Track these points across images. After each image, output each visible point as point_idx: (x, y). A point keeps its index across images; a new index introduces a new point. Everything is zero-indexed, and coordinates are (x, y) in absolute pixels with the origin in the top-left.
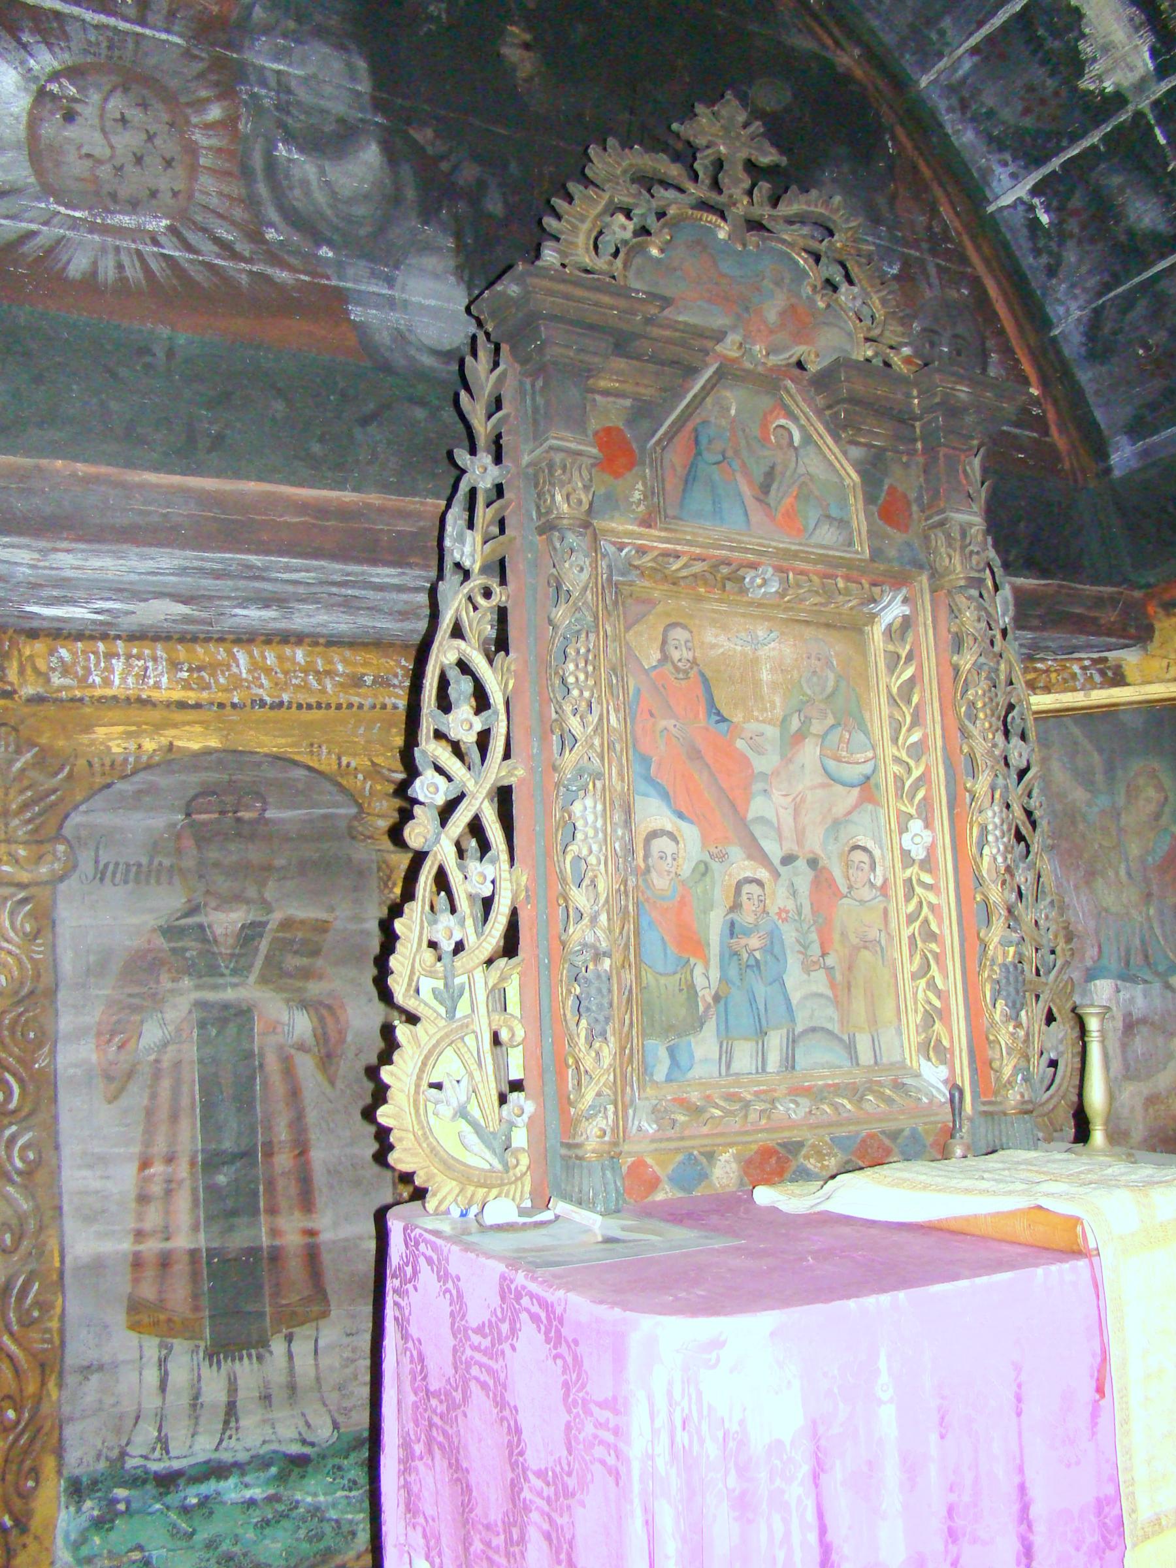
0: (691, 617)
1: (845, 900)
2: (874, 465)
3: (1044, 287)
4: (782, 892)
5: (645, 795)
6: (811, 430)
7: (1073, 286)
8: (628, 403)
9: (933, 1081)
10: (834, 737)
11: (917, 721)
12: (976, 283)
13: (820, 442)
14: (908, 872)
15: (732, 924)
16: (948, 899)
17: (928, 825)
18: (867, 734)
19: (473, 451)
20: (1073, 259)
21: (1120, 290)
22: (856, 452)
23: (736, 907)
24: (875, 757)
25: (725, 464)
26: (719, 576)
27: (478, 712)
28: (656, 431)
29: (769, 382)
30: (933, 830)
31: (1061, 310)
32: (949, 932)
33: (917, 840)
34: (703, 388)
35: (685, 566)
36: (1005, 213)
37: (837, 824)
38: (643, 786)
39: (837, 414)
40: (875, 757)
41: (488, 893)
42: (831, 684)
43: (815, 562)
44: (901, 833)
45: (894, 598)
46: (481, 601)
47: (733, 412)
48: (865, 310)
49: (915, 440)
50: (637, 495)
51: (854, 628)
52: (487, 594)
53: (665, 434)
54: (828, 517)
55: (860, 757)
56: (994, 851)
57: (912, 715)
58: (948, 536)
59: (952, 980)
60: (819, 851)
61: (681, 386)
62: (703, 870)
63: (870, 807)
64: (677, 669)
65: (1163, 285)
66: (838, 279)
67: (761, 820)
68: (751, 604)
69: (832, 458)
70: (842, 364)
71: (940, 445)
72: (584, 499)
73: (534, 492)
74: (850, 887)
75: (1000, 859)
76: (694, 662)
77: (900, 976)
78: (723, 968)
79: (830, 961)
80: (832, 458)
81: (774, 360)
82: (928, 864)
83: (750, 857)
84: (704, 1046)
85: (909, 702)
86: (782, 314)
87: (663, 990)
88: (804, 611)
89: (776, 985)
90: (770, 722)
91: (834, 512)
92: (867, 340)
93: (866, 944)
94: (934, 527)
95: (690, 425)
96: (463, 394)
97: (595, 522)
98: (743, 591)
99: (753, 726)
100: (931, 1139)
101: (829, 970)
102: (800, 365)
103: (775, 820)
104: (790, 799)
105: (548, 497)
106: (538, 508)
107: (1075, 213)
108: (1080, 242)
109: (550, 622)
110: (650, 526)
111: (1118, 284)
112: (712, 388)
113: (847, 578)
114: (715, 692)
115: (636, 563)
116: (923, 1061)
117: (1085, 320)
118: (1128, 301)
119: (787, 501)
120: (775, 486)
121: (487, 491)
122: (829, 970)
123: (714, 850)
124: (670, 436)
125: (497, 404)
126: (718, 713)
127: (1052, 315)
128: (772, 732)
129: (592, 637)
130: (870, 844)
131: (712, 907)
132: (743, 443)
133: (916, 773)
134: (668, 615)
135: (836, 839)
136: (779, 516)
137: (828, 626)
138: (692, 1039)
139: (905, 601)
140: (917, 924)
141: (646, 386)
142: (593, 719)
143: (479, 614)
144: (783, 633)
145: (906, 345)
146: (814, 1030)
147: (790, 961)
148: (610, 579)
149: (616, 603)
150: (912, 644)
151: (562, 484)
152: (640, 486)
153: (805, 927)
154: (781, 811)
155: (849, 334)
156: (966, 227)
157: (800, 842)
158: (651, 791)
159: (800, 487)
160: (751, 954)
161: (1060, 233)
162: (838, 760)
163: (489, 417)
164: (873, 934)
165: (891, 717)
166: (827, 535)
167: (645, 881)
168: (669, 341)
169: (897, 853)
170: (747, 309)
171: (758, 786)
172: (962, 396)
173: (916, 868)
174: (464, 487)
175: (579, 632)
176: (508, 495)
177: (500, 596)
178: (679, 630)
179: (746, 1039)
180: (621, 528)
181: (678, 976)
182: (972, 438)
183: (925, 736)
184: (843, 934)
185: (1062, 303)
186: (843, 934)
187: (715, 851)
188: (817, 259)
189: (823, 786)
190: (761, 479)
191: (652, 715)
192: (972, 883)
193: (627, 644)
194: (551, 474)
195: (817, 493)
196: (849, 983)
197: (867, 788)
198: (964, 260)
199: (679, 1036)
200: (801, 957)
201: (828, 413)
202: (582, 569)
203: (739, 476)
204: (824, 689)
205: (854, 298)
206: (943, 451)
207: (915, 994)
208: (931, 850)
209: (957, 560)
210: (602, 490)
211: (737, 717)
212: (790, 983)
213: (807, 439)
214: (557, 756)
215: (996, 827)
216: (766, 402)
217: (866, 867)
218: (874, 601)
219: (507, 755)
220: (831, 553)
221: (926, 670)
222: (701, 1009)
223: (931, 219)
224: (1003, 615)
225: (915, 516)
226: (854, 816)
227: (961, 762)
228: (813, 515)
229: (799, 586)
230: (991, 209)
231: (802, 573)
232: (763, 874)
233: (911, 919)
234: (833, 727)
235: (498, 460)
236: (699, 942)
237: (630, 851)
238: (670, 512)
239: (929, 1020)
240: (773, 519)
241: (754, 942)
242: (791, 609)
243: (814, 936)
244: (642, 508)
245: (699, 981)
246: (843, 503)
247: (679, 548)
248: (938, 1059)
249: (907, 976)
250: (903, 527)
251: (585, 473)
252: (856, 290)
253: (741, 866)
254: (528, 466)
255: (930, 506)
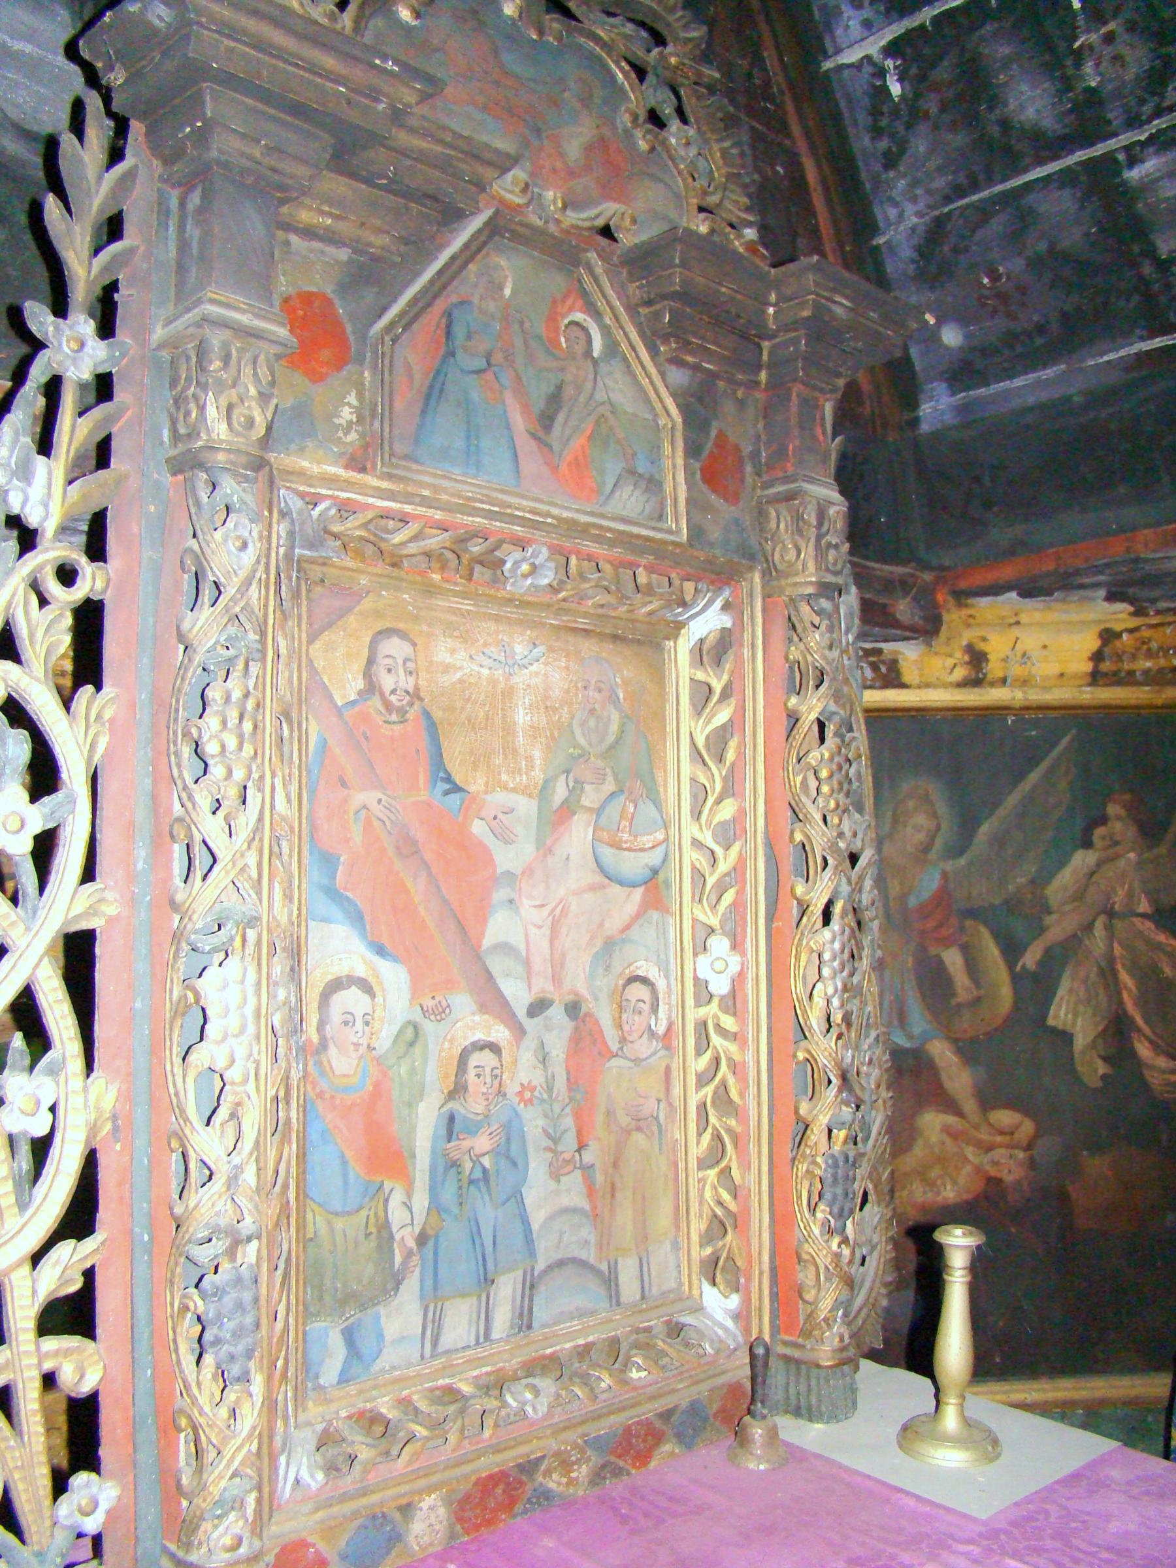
0: (416, 618)
1: (614, 1062)
2: (700, 400)
3: (877, 182)
4: (527, 1056)
5: (326, 920)
6: (620, 336)
7: (916, 182)
8: (343, 254)
9: (719, 1316)
10: (613, 810)
11: (731, 788)
12: (794, 163)
13: (630, 355)
14: (702, 1011)
15: (452, 1119)
16: (756, 1057)
17: (737, 946)
18: (658, 804)
19: (60, 309)
20: (922, 149)
21: (975, 197)
22: (678, 376)
23: (458, 1090)
24: (666, 840)
25: (489, 376)
26: (465, 558)
27: (35, 797)
28: (384, 309)
29: (562, 252)
30: (743, 954)
31: (892, 213)
32: (756, 1104)
33: (719, 965)
34: (466, 246)
35: (414, 538)
36: (846, 74)
37: (609, 946)
38: (323, 905)
39: (657, 315)
40: (666, 840)
41: (42, 1131)
42: (614, 728)
43: (612, 544)
44: (695, 954)
45: (711, 602)
46: (53, 587)
47: (507, 292)
48: (701, 163)
49: (759, 368)
50: (347, 414)
51: (648, 640)
52: (67, 575)
53: (402, 314)
54: (632, 472)
55: (646, 840)
56: (830, 991)
57: (725, 779)
58: (798, 518)
59: (756, 1179)
60: (584, 992)
61: (432, 238)
62: (411, 1036)
63: (655, 915)
64: (388, 706)
65: (1030, 199)
66: (668, 111)
67: (505, 948)
68: (509, 601)
69: (645, 382)
70: (674, 237)
71: (795, 380)
72: (259, 419)
73: (168, 397)
74: (623, 1040)
75: (836, 1002)
76: (415, 695)
77: (681, 1165)
78: (433, 1189)
79: (588, 1157)
80: (645, 382)
81: (573, 218)
82: (733, 1002)
83: (483, 1008)
84: (400, 1318)
85: (721, 759)
86: (588, 149)
87: (339, 1239)
88: (585, 615)
89: (511, 1206)
90: (525, 791)
91: (642, 467)
92: (701, 209)
93: (639, 1123)
94: (777, 500)
95: (440, 305)
96: (51, 202)
97: (272, 457)
98: (498, 580)
99: (499, 798)
100: (715, 1407)
101: (587, 1169)
102: (606, 232)
103: (522, 947)
104: (546, 911)
105: (192, 406)
106: (174, 423)
107: (936, 88)
108: (936, 128)
109: (181, 637)
110: (363, 470)
111: (975, 187)
112: (479, 250)
113: (650, 569)
114: (445, 745)
115: (336, 528)
116: (706, 1287)
117: (921, 230)
118: (984, 213)
119: (578, 442)
120: (561, 418)
121: (83, 386)
122: (587, 1169)
123: (429, 1003)
124: (409, 319)
125: (113, 228)
126: (448, 779)
127: (880, 218)
128: (526, 806)
129: (254, 669)
130: (653, 973)
131: (422, 1096)
132: (519, 342)
133: (723, 867)
134: (378, 614)
135: (608, 968)
136: (563, 467)
137: (615, 638)
138: (382, 1310)
139: (726, 607)
140: (709, 1090)
141: (379, 231)
142: (246, 821)
143: (50, 612)
144: (551, 649)
145: (750, 224)
146: (561, 1263)
147: (532, 1165)
148: (289, 556)
149: (296, 595)
150: (732, 673)
151: (221, 387)
152: (352, 399)
153: (557, 1108)
154: (533, 931)
155: (677, 196)
156: (792, 86)
157: (556, 979)
158: (339, 915)
159: (597, 423)
160: (476, 1161)
161: (911, 111)
162: (617, 845)
163: (97, 251)
164: (649, 1107)
165: (693, 780)
166: (629, 502)
167: (319, 1063)
168: (422, 157)
169: (689, 983)
170: (538, 131)
171: (500, 895)
172: (839, 311)
173: (714, 1007)
174: (38, 374)
175: (231, 661)
176: (121, 394)
177: (91, 580)
178: (396, 640)
179: (463, 1295)
180: (316, 469)
181: (364, 1213)
182: (838, 375)
183: (742, 812)
184: (610, 1113)
185: (896, 204)
186: (610, 1113)
187: (432, 1003)
188: (640, 72)
189: (592, 888)
190: (541, 405)
191: (344, 784)
192: (791, 1033)
193: (310, 662)
194: (201, 367)
195: (620, 434)
196: (613, 1187)
197: (654, 887)
198: (784, 129)
199: (363, 1308)
200: (549, 1155)
201: (643, 311)
202: (245, 546)
203: (510, 399)
204: (602, 740)
205: (688, 144)
206: (797, 389)
207: (701, 1191)
208: (738, 981)
209: (808, 553)
210: (289, 402)
211: (476, 784)
212: (531, 1196)
213: (612, 349)
214: (178, 882)
215: (834, 958)
216: (557, 282)
217: (646, 1007)
218: (683, 604)
219: (89, 874)
220: (636, 530)
221: (749, 714)
222: (398, 1259)
223: (752, 65)
224: (848, 631)
225: (749, 480)
226: (634, 933)
227: (788, 858)
228: (613, 468)
229: (582, 577)
230: (827, 65)
231: (590, 557)
232: (500, 1033)
233: (703, 1080)
234: (612, 794)
235: (106, 329)
236: (399, 1155)
237: (297, 1023)
238: (399, 448)
239: (718, 1227)
240: (554, 469)
241: (482, 1143)
242: (567, 611)
243: (568, 1122)
244: (353, 436)
245: (397, 1214)
246: (655, 457)
247: (408, 508)
248: (728, 1283)
249: (693, 1164)
250: (733, 498)
251: (263, 371)
252: (691, 132)
253: (470, 1023)
254: (160, 346)
255: (770, 468)
